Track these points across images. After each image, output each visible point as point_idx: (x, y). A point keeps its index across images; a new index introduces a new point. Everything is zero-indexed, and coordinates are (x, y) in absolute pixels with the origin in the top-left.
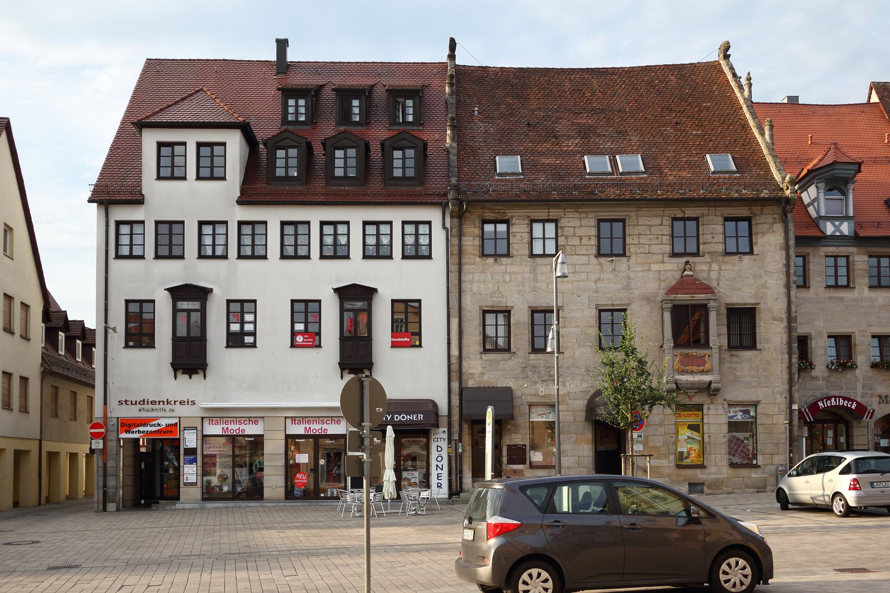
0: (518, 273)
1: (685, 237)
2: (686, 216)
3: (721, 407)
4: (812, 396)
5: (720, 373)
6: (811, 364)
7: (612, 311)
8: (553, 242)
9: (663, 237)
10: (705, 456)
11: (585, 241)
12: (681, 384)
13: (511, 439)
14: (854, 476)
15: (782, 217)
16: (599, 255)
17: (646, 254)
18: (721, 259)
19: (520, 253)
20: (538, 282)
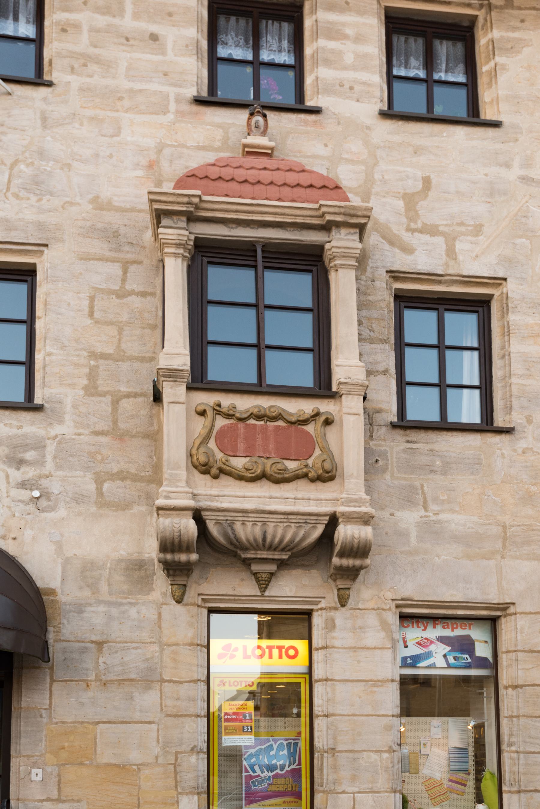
3: (372, 620)
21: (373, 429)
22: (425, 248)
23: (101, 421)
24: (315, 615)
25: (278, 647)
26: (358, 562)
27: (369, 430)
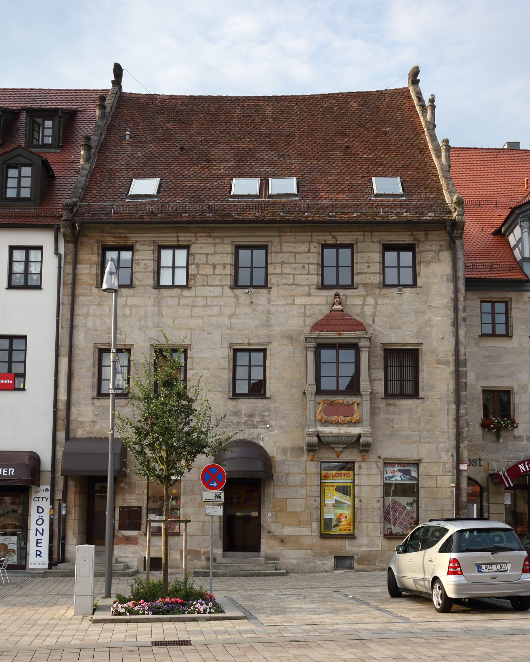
0: (140, 306)
1: (337, 267)
2: (338, 242)
3: (374, 465)
4: (514, 458)
5: (372, 424)
6: (513, 422)
7: (250, 351)
8: (184, 271)
9: (310, 266)
10: (356, 524)
11: (218, 270)
12: (324, 437)
13: (124, 500)
14: (454, 555)
15: (450, 244)
16: (236, 285)
17: (290, 285)
18: (377, 291)
19: (143, 283)
20: (162, 316)
24: (356, 463)
25: (343, 473)
26: (368, 449)
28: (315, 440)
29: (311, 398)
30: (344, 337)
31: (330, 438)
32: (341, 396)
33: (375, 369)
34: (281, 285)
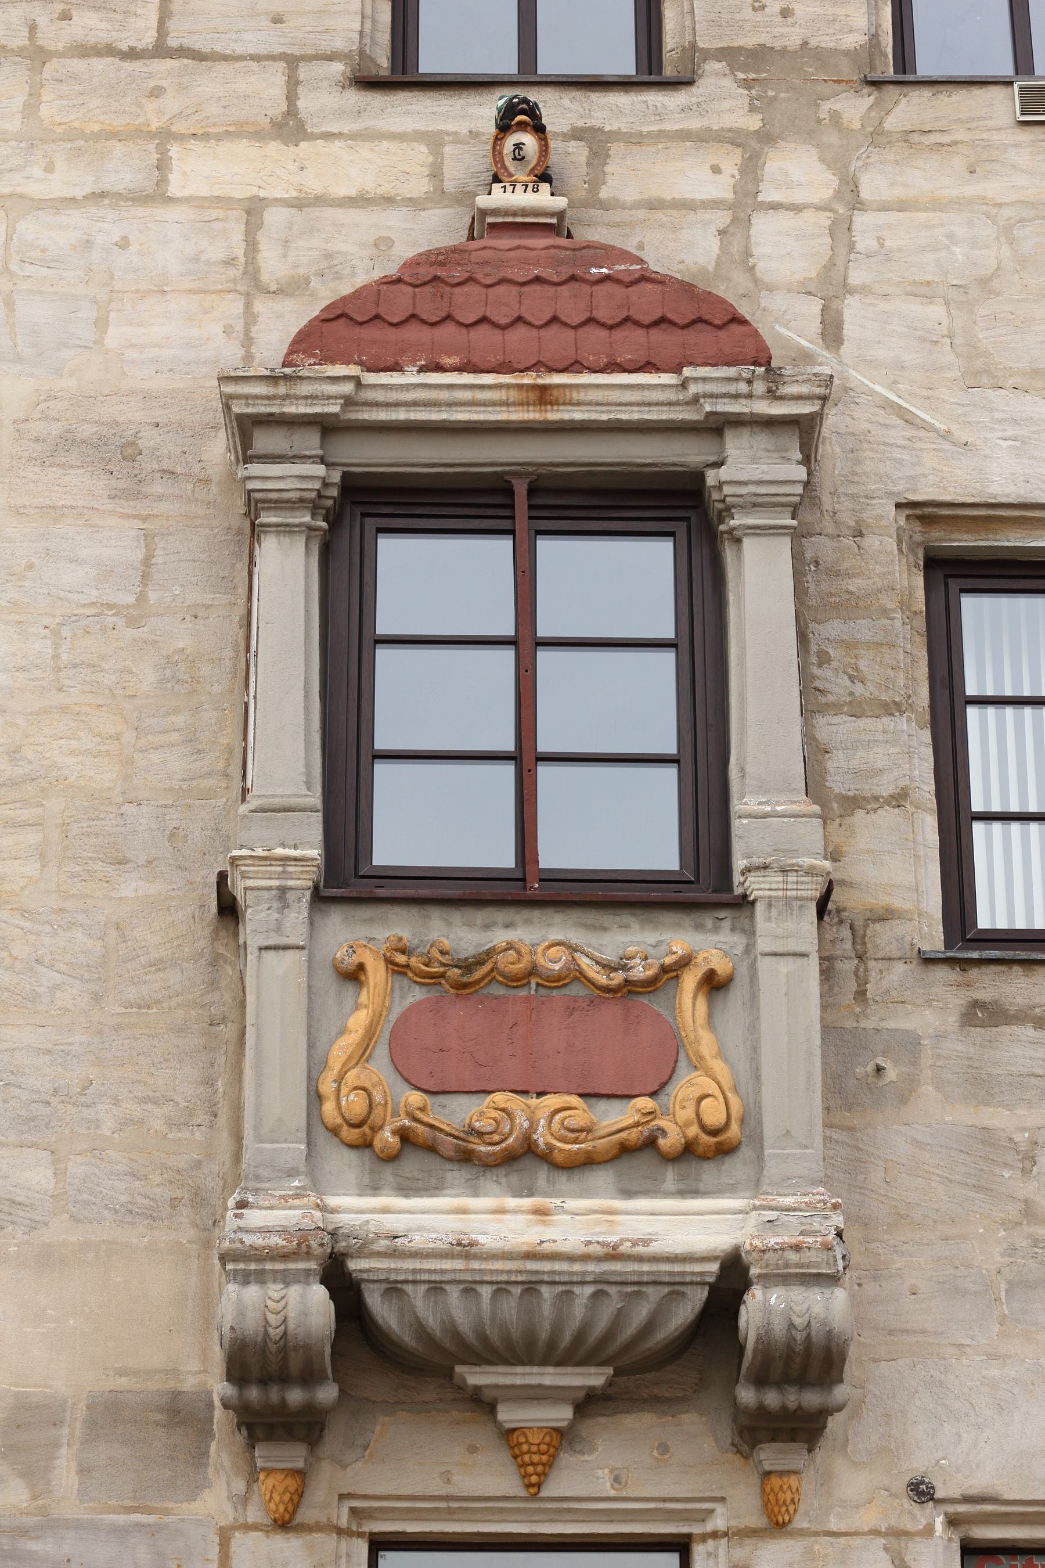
12: (393, 1289)
17: (132, 54)
21: (866, 970)
22: (1007, 434)
23: (71, 980)
26: (811, 1399)
27: (856, 974)
28: (305, 1313)
29: (279, 928)
30: (565, 416)
31: (454, 1293)
32: (558, 917)
33: (857, 709)
34: (60, 55)
